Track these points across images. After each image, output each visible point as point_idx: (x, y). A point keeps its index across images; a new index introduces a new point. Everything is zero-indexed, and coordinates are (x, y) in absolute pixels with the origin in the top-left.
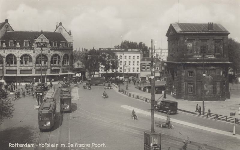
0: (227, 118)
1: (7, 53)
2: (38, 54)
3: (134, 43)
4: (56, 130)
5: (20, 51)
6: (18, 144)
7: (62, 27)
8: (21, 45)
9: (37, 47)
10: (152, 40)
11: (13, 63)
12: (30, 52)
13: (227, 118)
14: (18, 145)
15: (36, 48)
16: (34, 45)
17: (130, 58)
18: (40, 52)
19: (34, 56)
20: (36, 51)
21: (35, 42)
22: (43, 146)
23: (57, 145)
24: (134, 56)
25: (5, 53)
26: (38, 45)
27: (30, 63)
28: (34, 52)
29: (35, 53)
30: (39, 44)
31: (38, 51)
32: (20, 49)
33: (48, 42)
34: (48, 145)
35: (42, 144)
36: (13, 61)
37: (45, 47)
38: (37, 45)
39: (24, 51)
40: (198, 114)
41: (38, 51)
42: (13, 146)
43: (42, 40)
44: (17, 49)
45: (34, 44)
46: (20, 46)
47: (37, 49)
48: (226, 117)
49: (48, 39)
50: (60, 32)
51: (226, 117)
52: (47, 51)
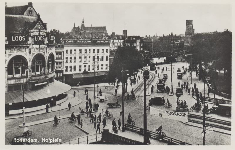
0: (172, 140)
2: (35, 54)
3: (65, 33)
7: (32, 9)
10: (230, 135)
12: (24, 53)
13: (172, 140)
15: (33, 45)
16: (30, 41)
17: (80, 53)
18: (38, 52)
21: (32, 34)
22: (47, 141)
23: (59, 140)
24: (80, 50)
26: (34, 40)
28: (30, 52)
29: (32, 54)
30: (37, 39)
31: (35, 50)
34: (52, 140)
35: (45, 139)
39: (15, 52)
41: (35, 50)
42: (18, 141)
47: (33, 46)
48: (170, 139)
51: (172, 138)
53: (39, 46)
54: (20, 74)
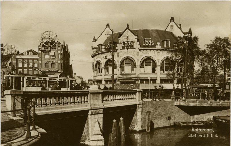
1: (141, 56)
4: (209, 113)
5: (161, 53)
6: (199, 129)
8: (162, 45)
9: (121, 48)
11: (48, 82)
14: (192, 136)
16: (119, 46)
19: (138, 59)
20: (120, 54)
25: (139, 56)
27: (141, 69)
32: (161, 50)
33: (136, 40)
36: (164, 66)
37: (132, 47)
38: (121, 46)
40: (148, 131)
43: (128, 38)
44: (157, 50)
45: (118, 45)
46: (140, 46)
49: (136, 36)
50: (171, 32)
52: (135, 54)
53: (128, 50)
54: (66, 88)
